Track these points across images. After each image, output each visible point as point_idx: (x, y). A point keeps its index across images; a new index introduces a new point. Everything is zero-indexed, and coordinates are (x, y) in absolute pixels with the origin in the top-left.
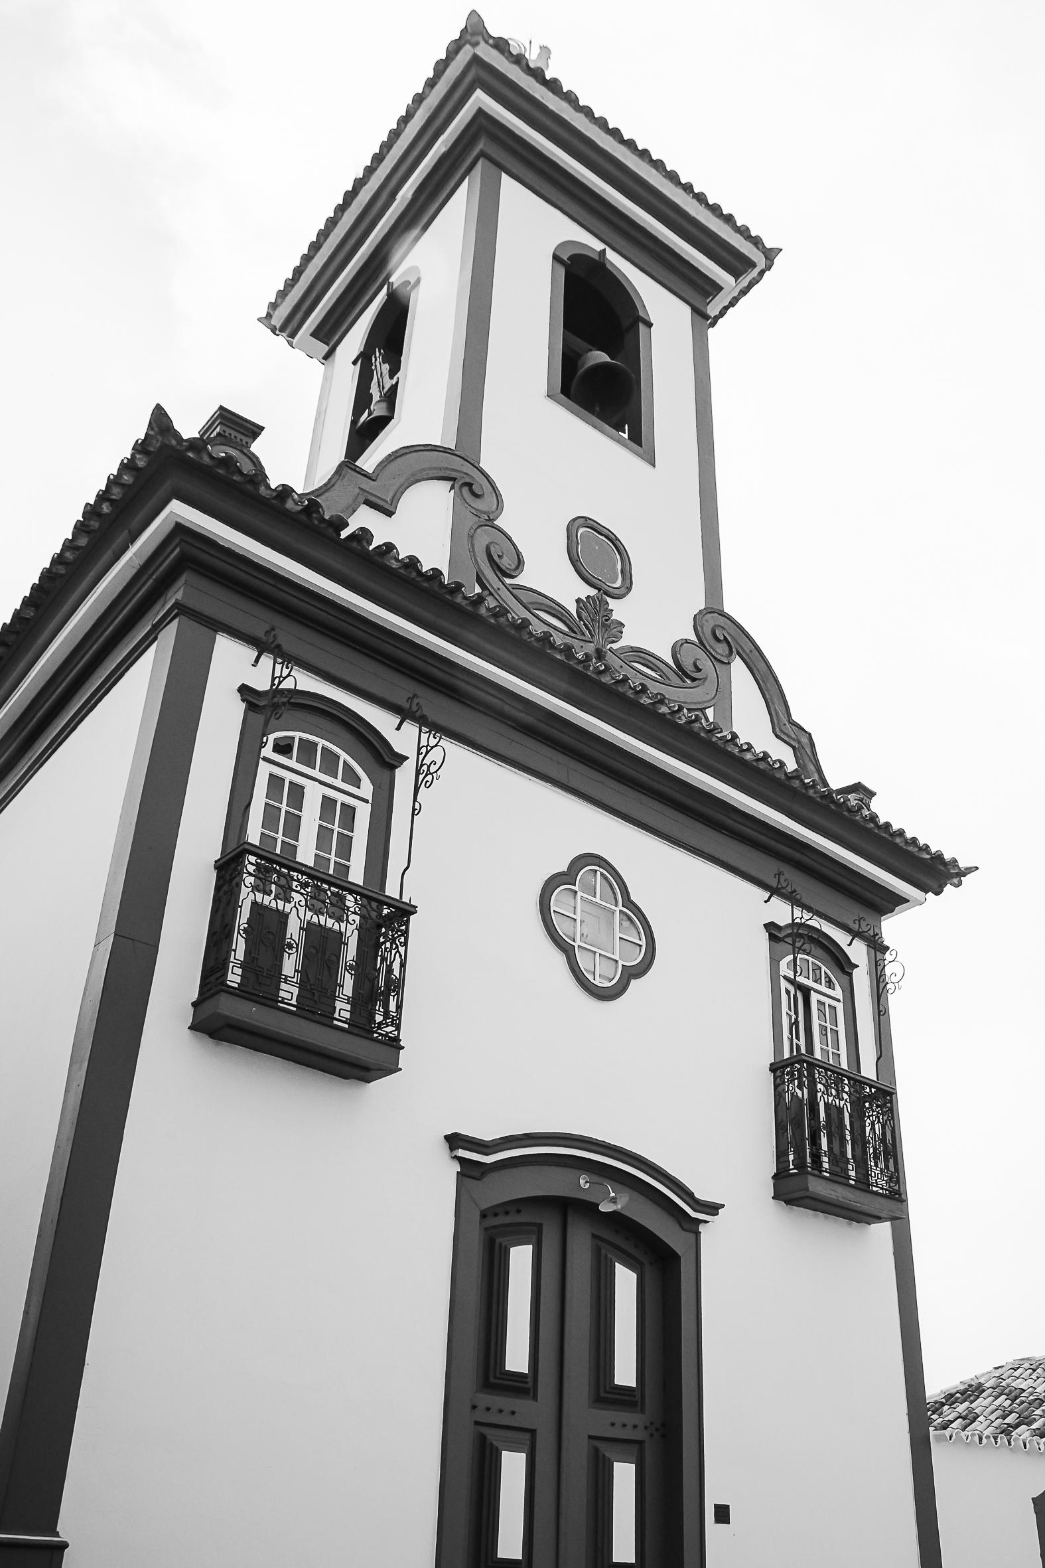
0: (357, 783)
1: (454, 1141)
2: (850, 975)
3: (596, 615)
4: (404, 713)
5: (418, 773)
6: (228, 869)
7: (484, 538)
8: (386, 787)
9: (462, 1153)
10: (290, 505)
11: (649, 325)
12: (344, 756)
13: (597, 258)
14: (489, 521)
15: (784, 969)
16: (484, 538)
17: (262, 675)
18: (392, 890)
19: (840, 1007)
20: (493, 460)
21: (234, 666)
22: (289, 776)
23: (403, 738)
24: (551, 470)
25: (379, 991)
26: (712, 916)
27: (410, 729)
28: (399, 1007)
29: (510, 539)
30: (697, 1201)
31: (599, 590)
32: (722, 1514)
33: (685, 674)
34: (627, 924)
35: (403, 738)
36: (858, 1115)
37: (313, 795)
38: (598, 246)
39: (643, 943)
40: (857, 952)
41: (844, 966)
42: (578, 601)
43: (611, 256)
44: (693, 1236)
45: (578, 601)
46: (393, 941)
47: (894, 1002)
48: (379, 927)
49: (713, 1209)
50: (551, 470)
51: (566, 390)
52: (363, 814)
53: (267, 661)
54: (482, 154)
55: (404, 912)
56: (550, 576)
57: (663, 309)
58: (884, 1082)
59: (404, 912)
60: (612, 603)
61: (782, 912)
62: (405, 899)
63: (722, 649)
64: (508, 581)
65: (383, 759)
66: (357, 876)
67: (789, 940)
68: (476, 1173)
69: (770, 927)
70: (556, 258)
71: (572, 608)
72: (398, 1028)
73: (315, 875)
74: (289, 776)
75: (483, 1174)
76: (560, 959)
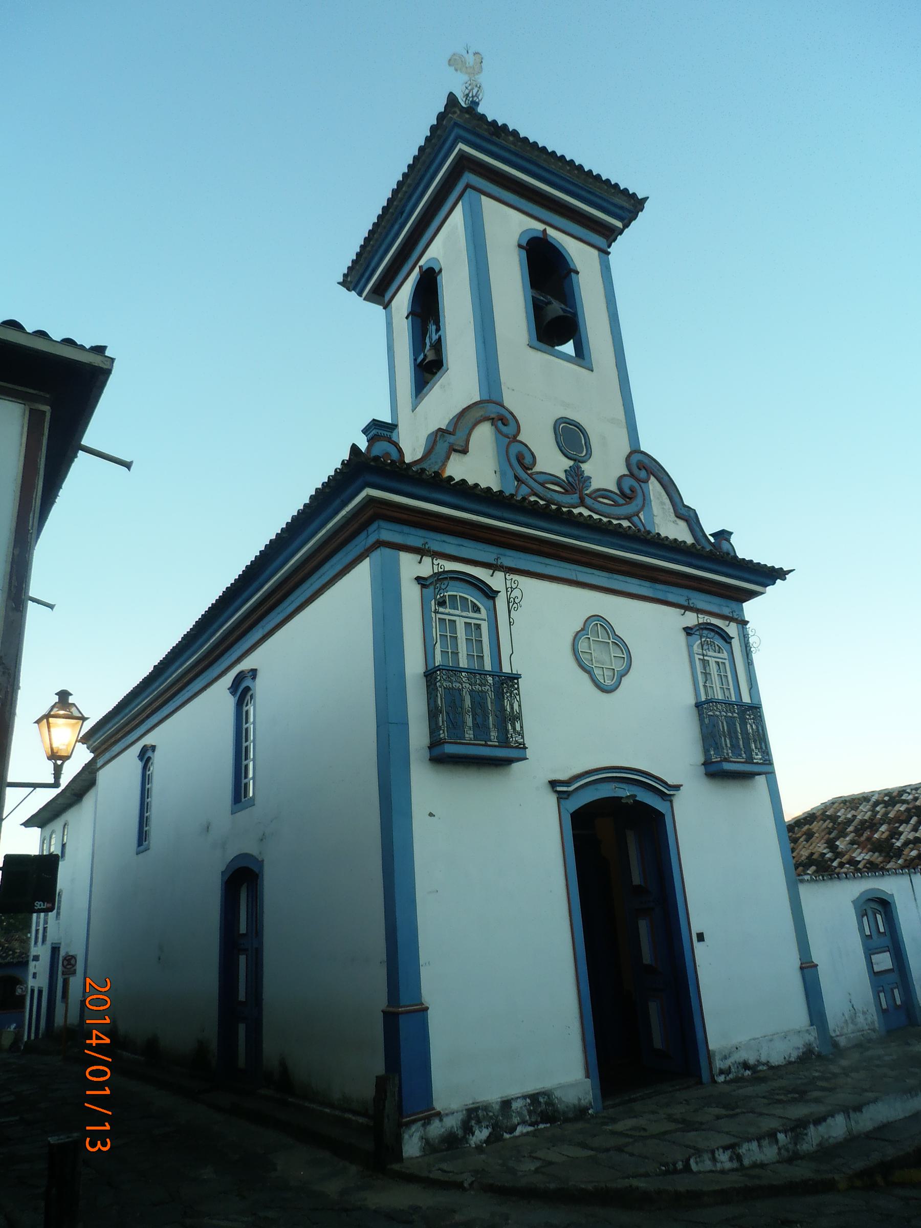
0: (478, 610)
1: (553, 784)
2: (730, 643)
3: (576, 481)
4: (493, 567)
5: (509, 603)
6: (430, 675)
7: (514, 449)
8: (492, 608)
9: (559, 789)
10: (424, 476)
11: (577, 273)
12: (470, 598)
13: (541, 236)
14: (514, 439)
15: (696, 648)
16: (514, 449)
17: (426, 568)
18: (506, 669)
19: (727, 662)
20: (510, 401)
21: (411, 567)
22: (447, 617)
23: (496, 581)
24: (540, 387)
25: (509, 720)
26: (653, 628)
27: (500, 575)
28: (522, 727)
29: (526, 446)
30: (670, 786)
31: (575, 460)
32: (701, 937)
33: (627, 496)
34: (615, 647)
35: (496, 581)
36: (744, 723)
37: (460, 624)
38: (540, 227)
39: (625, 656)
40: (732, 630)
41: (727, 639)
42: (566, 471)
43: (551, 232)
44: (668, 803)
45: (566, 471)
46: (511, 692)
47: (756, 657)
48: (502, 684)
49: (677, 787)
50: (540, 387)
51: (540, 339)
52: (484, 626)
53: (427, 560)
54: (468, 186)
55: (513, 678)
56: (552, 462)
57: (578, 252)
58: (755, 702)
59: (513, 678)
60: (582, 465)
61: (691, 619)
62: (514, 672)
63: (643, 474)
64: (529, 472)
65: (490, 594)
66: (488, 666)
67: (697, 633)
68: (565, 796)
69: (688, 631)
70: (520, 246)
71: (563, 476)
72: (523, 737)
73: (471, 672)
74: (447, 617)
75: (569, 795)
76: (585, 676)
